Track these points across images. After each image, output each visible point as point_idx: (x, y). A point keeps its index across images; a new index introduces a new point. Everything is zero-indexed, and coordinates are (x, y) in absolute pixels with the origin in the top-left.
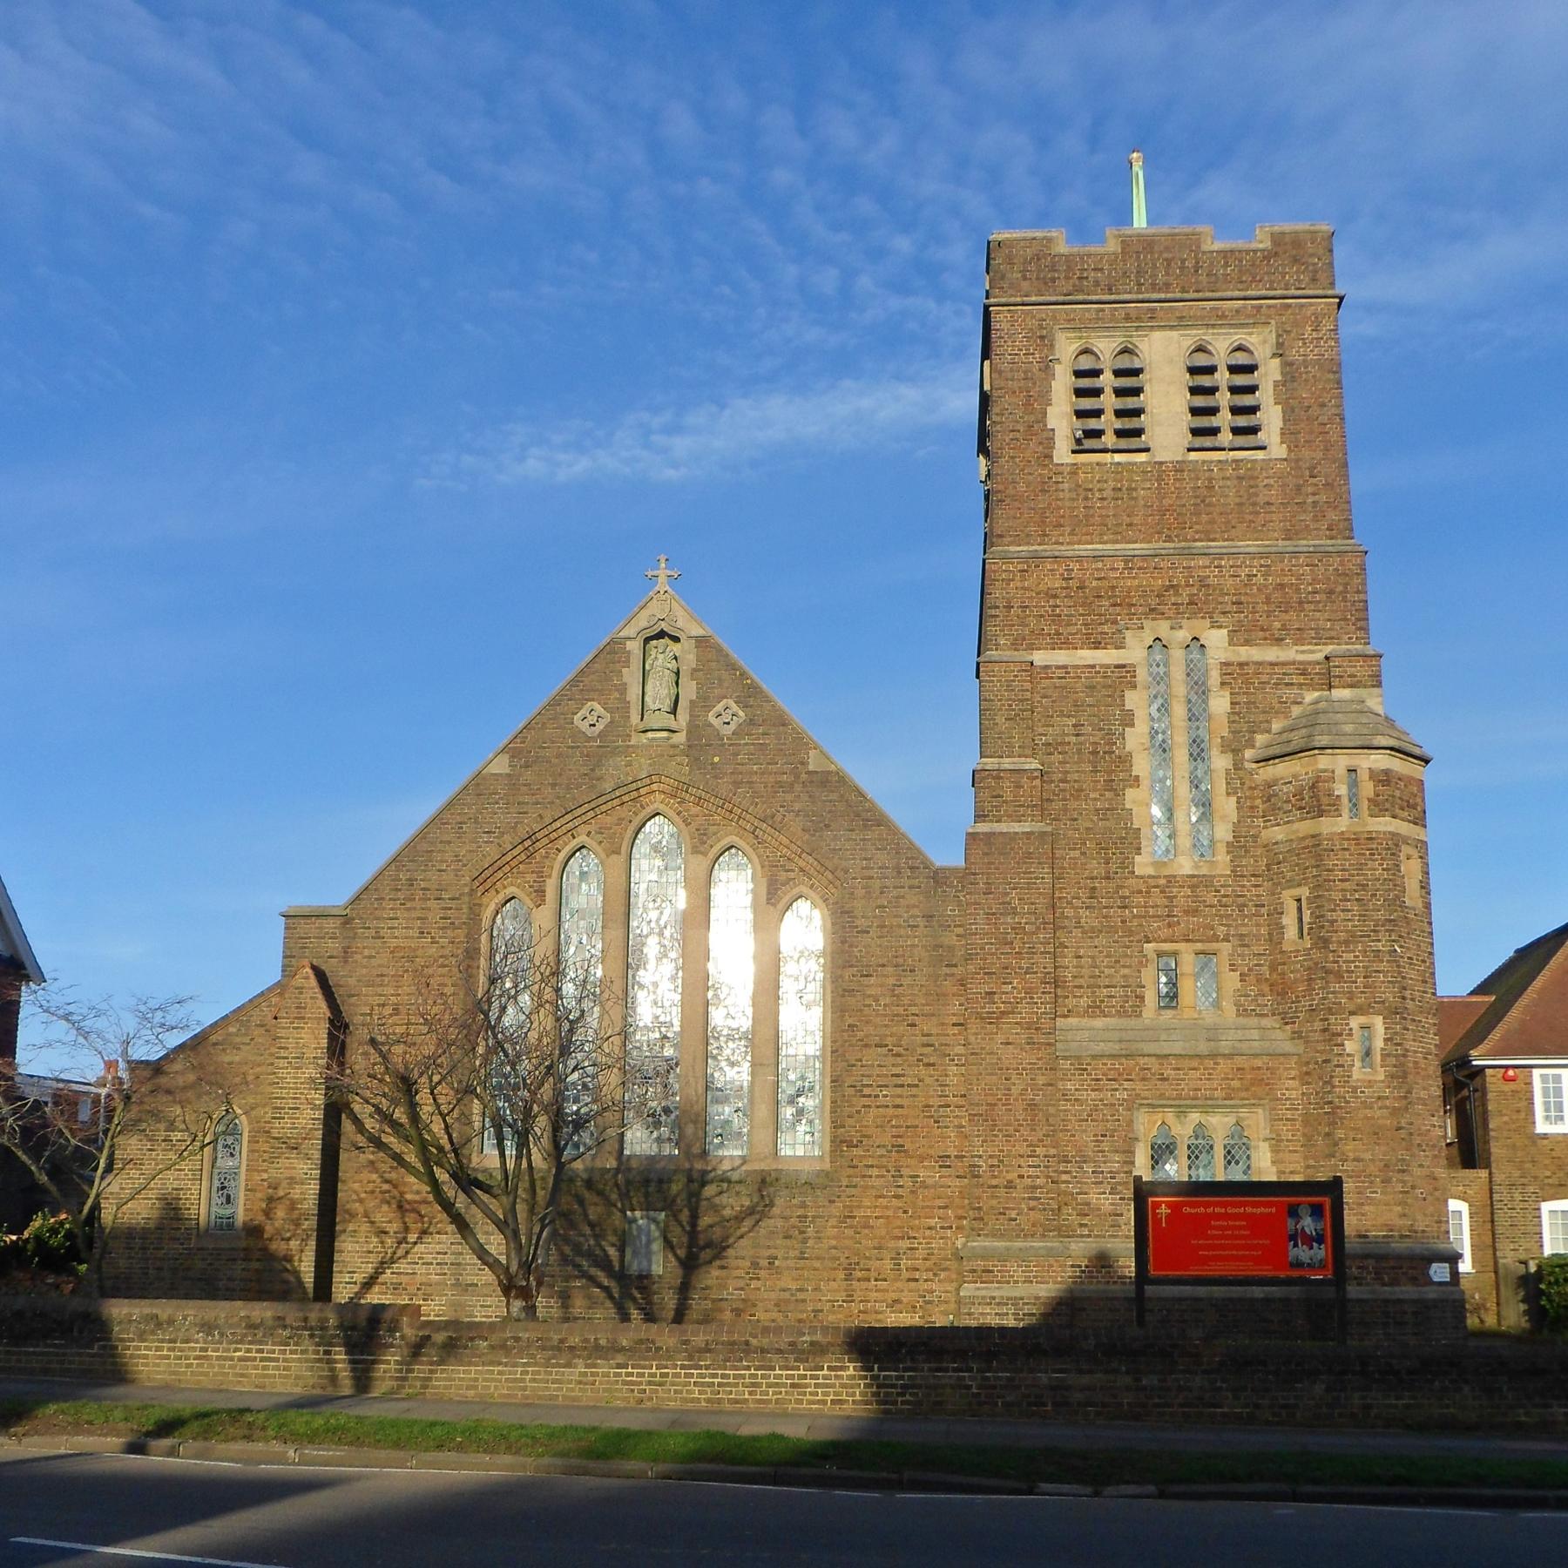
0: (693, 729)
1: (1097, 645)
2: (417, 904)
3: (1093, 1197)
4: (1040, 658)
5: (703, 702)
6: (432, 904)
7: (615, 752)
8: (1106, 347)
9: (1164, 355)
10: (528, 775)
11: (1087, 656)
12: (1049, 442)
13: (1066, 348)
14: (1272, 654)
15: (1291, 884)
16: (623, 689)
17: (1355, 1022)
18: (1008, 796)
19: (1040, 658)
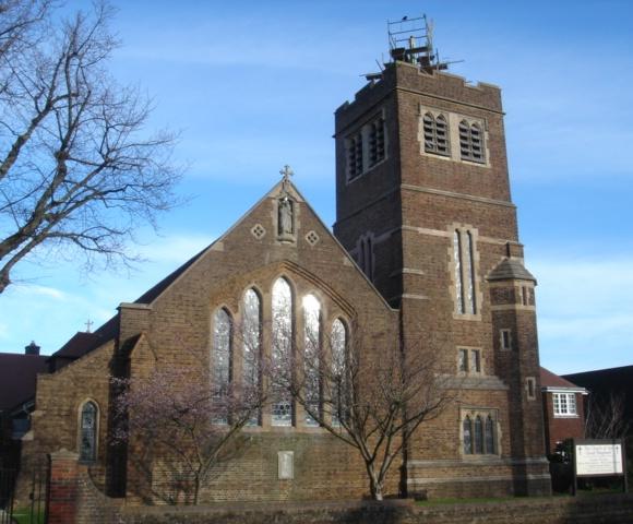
0: (300, 242)
1: (438, 229)
2: (184, 307)
3: (448, 444)
4: (421, 230)
5: (303, 232)
6: (191, 308)
7: (269, 247)
8: (436, 114)
9: (454, 120)
10: (231, 253)
11: (435, 232)
12: (418, 147)
13: (423, 111)
14: (491, 241)
15: (503, 327)
16: (271, 220)
17: (528, 379)
18: (414, 283)
19: (421, 230)
